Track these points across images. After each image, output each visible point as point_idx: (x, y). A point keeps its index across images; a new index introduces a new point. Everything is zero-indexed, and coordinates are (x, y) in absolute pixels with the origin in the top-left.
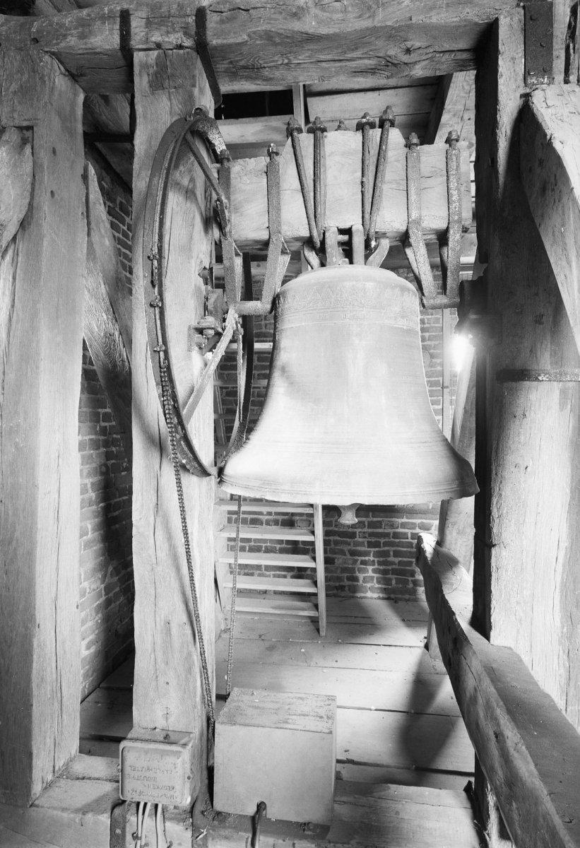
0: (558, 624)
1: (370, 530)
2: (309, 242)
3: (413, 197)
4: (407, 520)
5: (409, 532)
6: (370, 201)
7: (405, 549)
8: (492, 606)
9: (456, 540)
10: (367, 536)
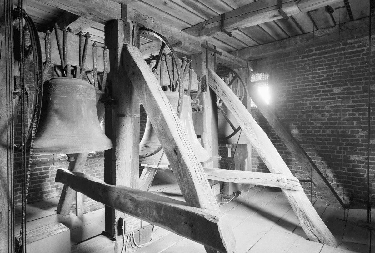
0: (130, 176)
1: (18, 175)
2: (60, 67)
3: (95, 62)
4: (38, 167)
5: (39, 172)
6: (82, 58)
7: (37, 180)
8: (116, 176)
9: (79, 167)
10: (17, 178)
